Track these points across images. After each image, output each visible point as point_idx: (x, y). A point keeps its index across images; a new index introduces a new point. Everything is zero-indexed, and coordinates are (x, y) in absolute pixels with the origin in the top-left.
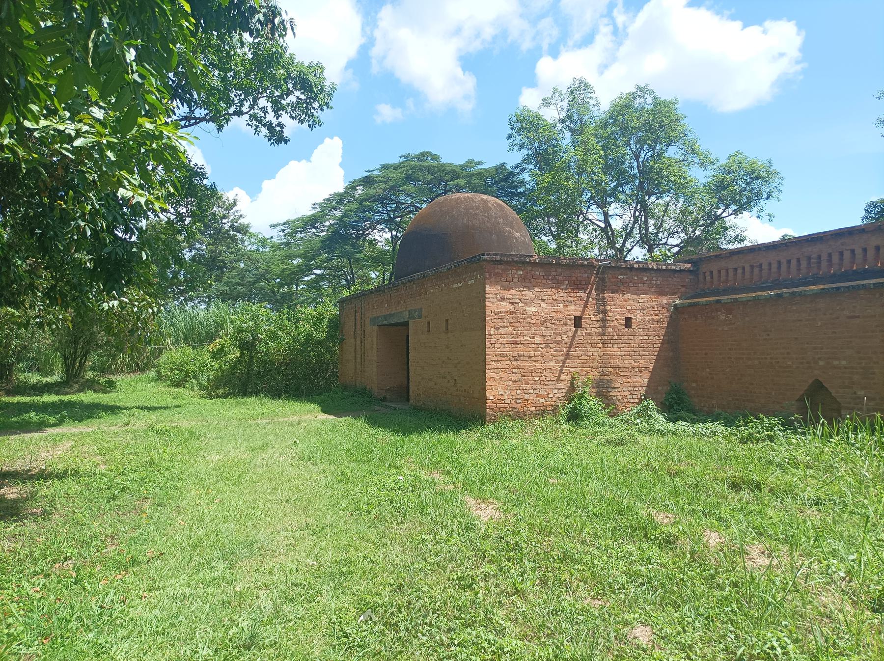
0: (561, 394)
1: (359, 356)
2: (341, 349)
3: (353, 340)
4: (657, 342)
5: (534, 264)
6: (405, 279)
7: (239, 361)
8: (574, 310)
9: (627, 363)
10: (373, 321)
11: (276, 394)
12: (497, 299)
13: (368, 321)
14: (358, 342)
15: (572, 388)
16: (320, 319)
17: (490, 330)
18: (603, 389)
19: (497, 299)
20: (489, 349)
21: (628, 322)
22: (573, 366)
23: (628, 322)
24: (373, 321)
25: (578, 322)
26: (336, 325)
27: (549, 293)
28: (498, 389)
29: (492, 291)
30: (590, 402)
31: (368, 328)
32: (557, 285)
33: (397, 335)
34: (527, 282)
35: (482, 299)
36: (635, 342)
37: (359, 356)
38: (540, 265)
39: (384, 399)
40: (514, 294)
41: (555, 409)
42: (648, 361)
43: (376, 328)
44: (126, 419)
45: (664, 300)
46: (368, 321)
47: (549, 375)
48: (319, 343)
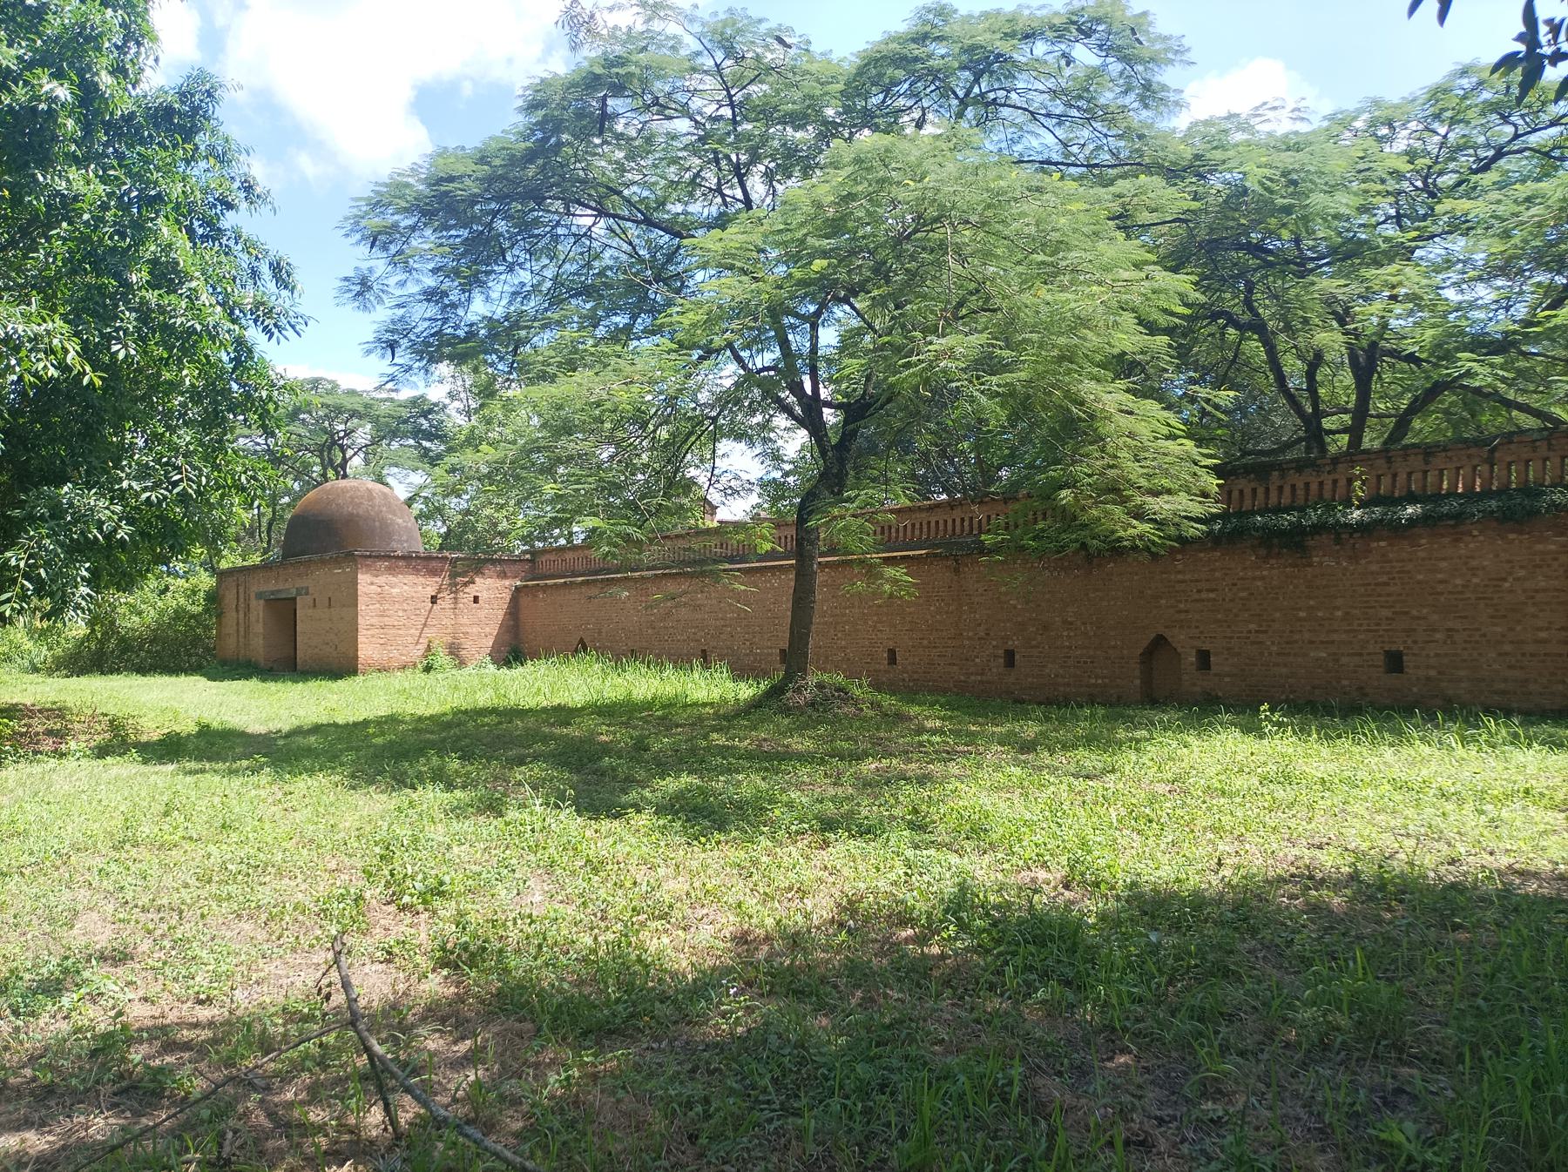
0: (420, 653)
1: (242, 630)
2: (219, 623)
3: (234, 614)
4: (500, 615)
5: (398, 557)
6: (293, 560)
7: (87, 638)
8: (431, 591)
9: (475, 630)
10: (259, 596)
11: (142, 670)
12: (367, 584)
13: (253, 596)
14: (241, 615)
15: (429, 648)
16: (194, 593)
17: (361, 607)
18: (454, 650)
19: (367, 584)
20: (360, 620)
21: (476, 600)
22: (429, 633)
23: (476, 600)
24: (259, 596)
25: (434, 600)
26: (213, 597)
27: (411, 579)
28: (367, 650)
29: (364, 579)
30: (442, 658)
31: (254, 603)
32: (416, 571)
33: (284, 611)
34: (391, 570)
35: (355, 583)
36: (482, 614)
37: (242, 630)
38: (403, 558)
39: (271, 670)
40: (382, 580)
41: (415, 665)
42: (493, 629)
43: (262, 602)
44: (151, 62)
45: (507, 582)
46: (253, 596)
47: (410, 639)
48: (193, 616)
